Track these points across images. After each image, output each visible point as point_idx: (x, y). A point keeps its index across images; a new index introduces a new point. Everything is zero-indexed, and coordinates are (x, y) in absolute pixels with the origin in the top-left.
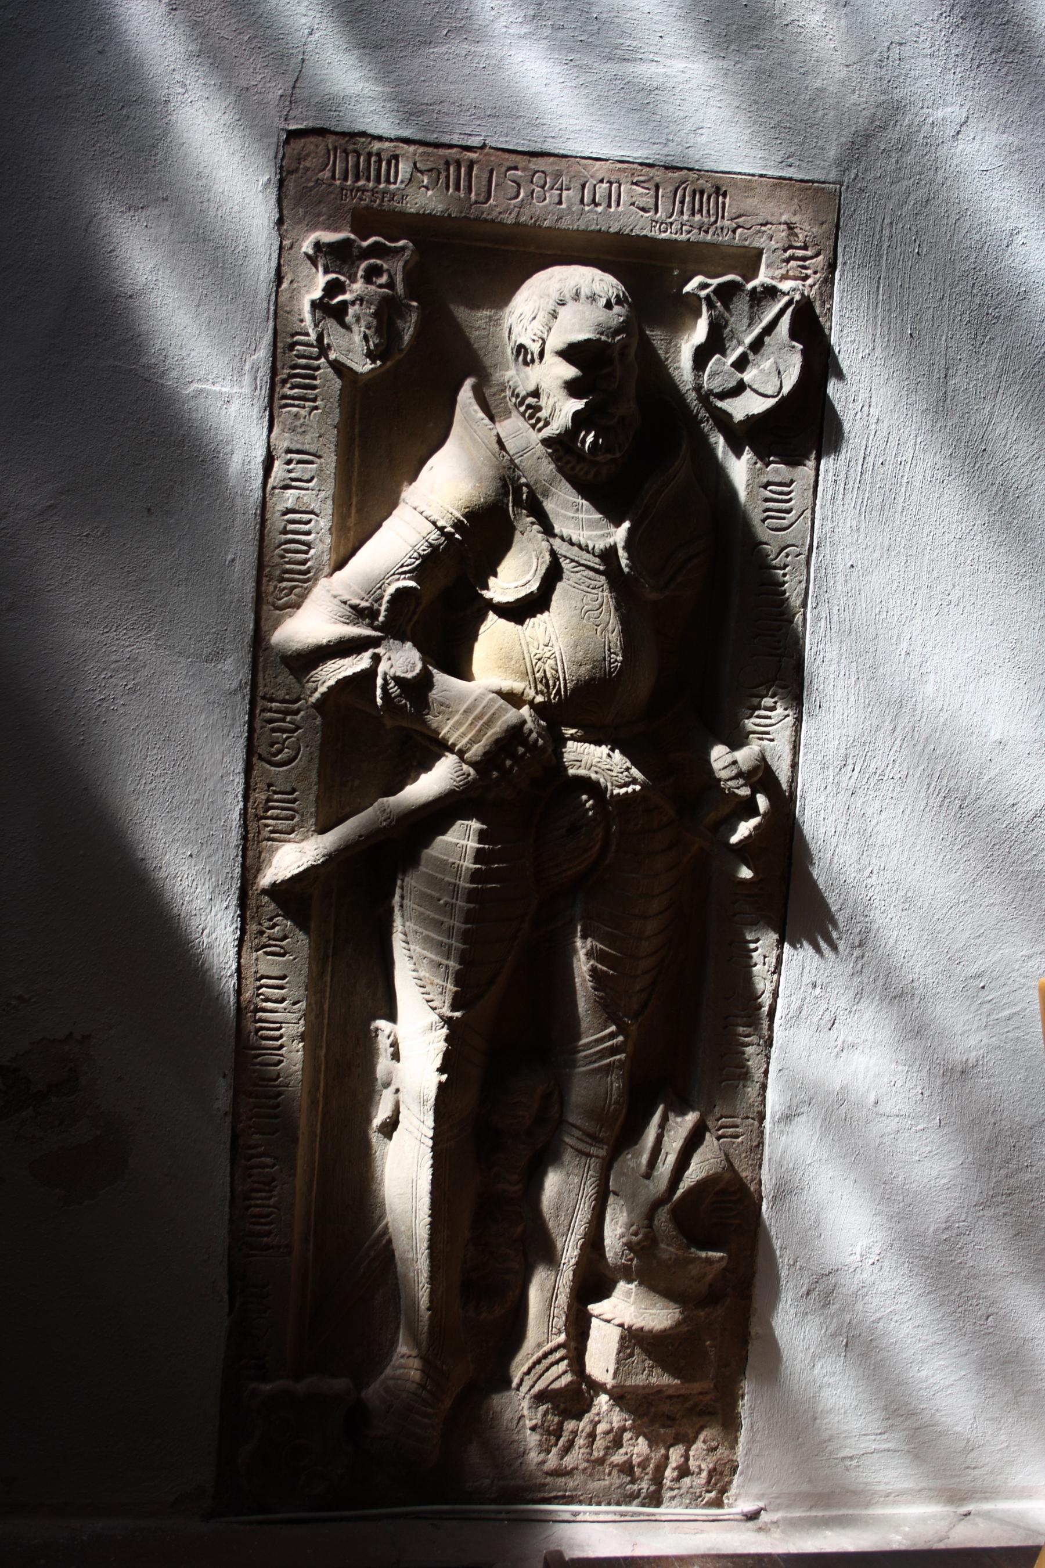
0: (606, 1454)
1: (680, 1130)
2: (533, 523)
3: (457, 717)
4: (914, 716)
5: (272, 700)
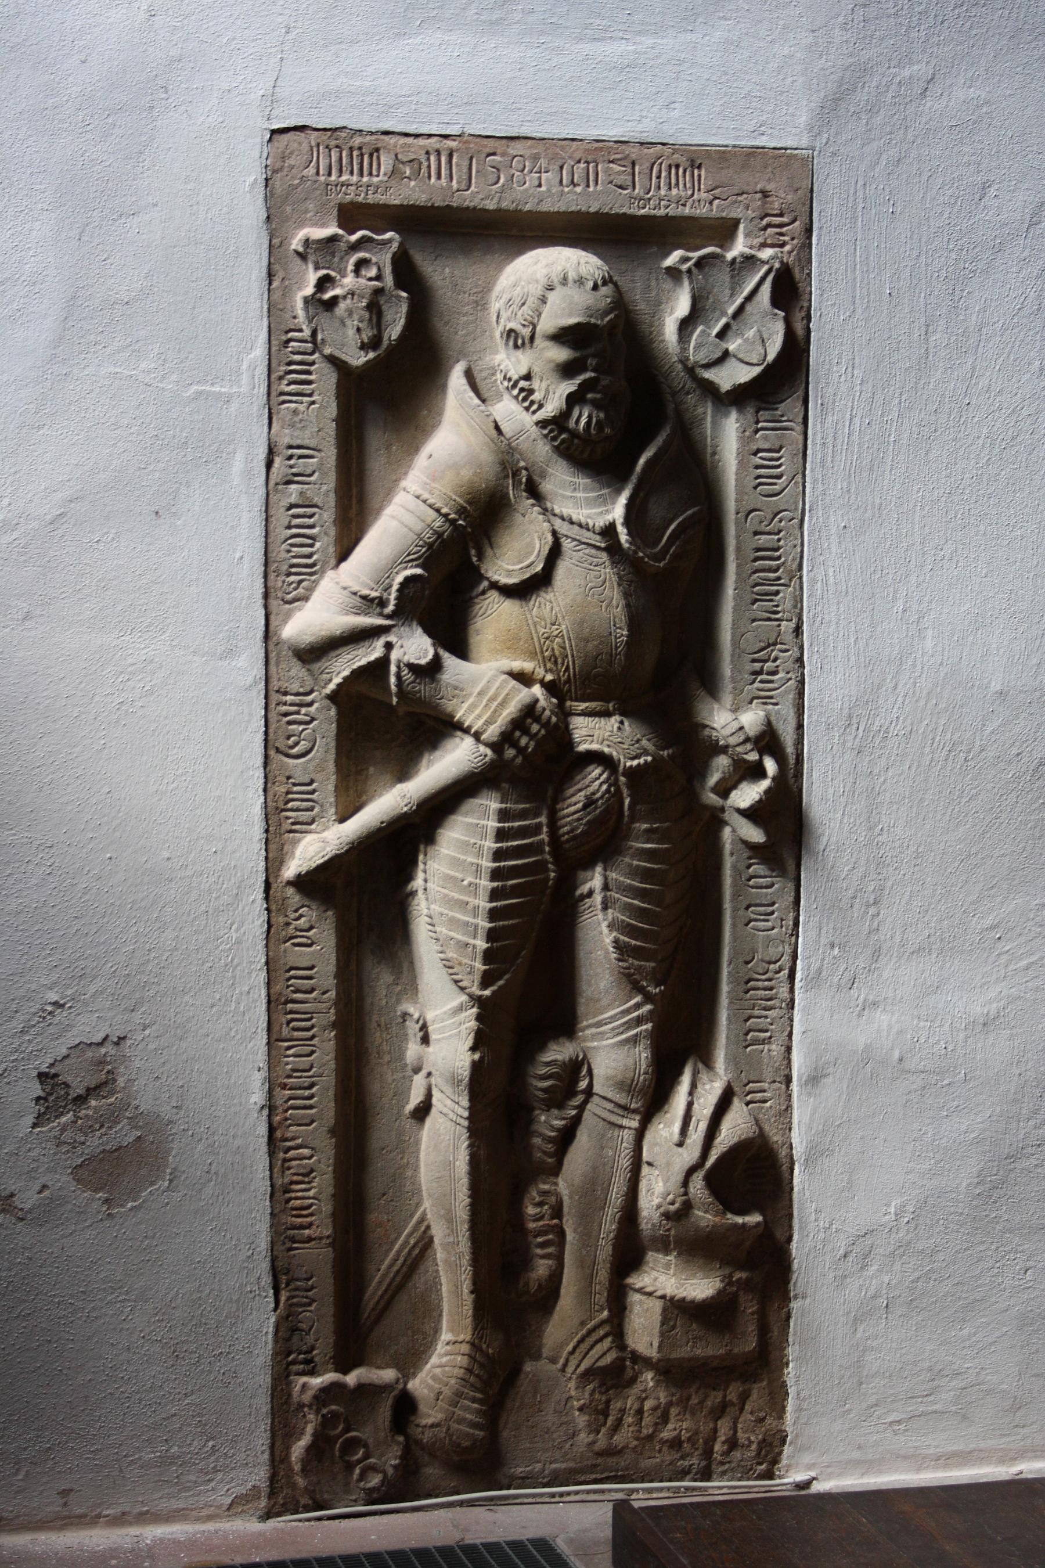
0: (654, 1431)
1: (710, 1097)
2: (533, 505)
3: (471, 700)
4: (914, 672)
5: (285, 694)
